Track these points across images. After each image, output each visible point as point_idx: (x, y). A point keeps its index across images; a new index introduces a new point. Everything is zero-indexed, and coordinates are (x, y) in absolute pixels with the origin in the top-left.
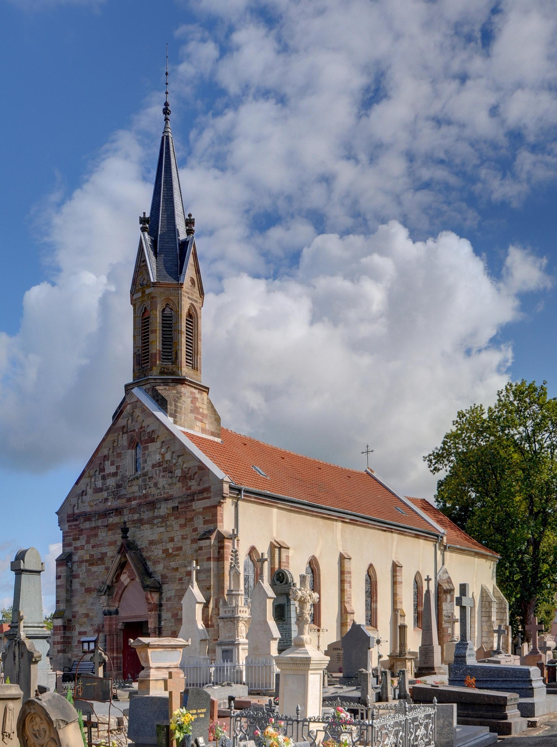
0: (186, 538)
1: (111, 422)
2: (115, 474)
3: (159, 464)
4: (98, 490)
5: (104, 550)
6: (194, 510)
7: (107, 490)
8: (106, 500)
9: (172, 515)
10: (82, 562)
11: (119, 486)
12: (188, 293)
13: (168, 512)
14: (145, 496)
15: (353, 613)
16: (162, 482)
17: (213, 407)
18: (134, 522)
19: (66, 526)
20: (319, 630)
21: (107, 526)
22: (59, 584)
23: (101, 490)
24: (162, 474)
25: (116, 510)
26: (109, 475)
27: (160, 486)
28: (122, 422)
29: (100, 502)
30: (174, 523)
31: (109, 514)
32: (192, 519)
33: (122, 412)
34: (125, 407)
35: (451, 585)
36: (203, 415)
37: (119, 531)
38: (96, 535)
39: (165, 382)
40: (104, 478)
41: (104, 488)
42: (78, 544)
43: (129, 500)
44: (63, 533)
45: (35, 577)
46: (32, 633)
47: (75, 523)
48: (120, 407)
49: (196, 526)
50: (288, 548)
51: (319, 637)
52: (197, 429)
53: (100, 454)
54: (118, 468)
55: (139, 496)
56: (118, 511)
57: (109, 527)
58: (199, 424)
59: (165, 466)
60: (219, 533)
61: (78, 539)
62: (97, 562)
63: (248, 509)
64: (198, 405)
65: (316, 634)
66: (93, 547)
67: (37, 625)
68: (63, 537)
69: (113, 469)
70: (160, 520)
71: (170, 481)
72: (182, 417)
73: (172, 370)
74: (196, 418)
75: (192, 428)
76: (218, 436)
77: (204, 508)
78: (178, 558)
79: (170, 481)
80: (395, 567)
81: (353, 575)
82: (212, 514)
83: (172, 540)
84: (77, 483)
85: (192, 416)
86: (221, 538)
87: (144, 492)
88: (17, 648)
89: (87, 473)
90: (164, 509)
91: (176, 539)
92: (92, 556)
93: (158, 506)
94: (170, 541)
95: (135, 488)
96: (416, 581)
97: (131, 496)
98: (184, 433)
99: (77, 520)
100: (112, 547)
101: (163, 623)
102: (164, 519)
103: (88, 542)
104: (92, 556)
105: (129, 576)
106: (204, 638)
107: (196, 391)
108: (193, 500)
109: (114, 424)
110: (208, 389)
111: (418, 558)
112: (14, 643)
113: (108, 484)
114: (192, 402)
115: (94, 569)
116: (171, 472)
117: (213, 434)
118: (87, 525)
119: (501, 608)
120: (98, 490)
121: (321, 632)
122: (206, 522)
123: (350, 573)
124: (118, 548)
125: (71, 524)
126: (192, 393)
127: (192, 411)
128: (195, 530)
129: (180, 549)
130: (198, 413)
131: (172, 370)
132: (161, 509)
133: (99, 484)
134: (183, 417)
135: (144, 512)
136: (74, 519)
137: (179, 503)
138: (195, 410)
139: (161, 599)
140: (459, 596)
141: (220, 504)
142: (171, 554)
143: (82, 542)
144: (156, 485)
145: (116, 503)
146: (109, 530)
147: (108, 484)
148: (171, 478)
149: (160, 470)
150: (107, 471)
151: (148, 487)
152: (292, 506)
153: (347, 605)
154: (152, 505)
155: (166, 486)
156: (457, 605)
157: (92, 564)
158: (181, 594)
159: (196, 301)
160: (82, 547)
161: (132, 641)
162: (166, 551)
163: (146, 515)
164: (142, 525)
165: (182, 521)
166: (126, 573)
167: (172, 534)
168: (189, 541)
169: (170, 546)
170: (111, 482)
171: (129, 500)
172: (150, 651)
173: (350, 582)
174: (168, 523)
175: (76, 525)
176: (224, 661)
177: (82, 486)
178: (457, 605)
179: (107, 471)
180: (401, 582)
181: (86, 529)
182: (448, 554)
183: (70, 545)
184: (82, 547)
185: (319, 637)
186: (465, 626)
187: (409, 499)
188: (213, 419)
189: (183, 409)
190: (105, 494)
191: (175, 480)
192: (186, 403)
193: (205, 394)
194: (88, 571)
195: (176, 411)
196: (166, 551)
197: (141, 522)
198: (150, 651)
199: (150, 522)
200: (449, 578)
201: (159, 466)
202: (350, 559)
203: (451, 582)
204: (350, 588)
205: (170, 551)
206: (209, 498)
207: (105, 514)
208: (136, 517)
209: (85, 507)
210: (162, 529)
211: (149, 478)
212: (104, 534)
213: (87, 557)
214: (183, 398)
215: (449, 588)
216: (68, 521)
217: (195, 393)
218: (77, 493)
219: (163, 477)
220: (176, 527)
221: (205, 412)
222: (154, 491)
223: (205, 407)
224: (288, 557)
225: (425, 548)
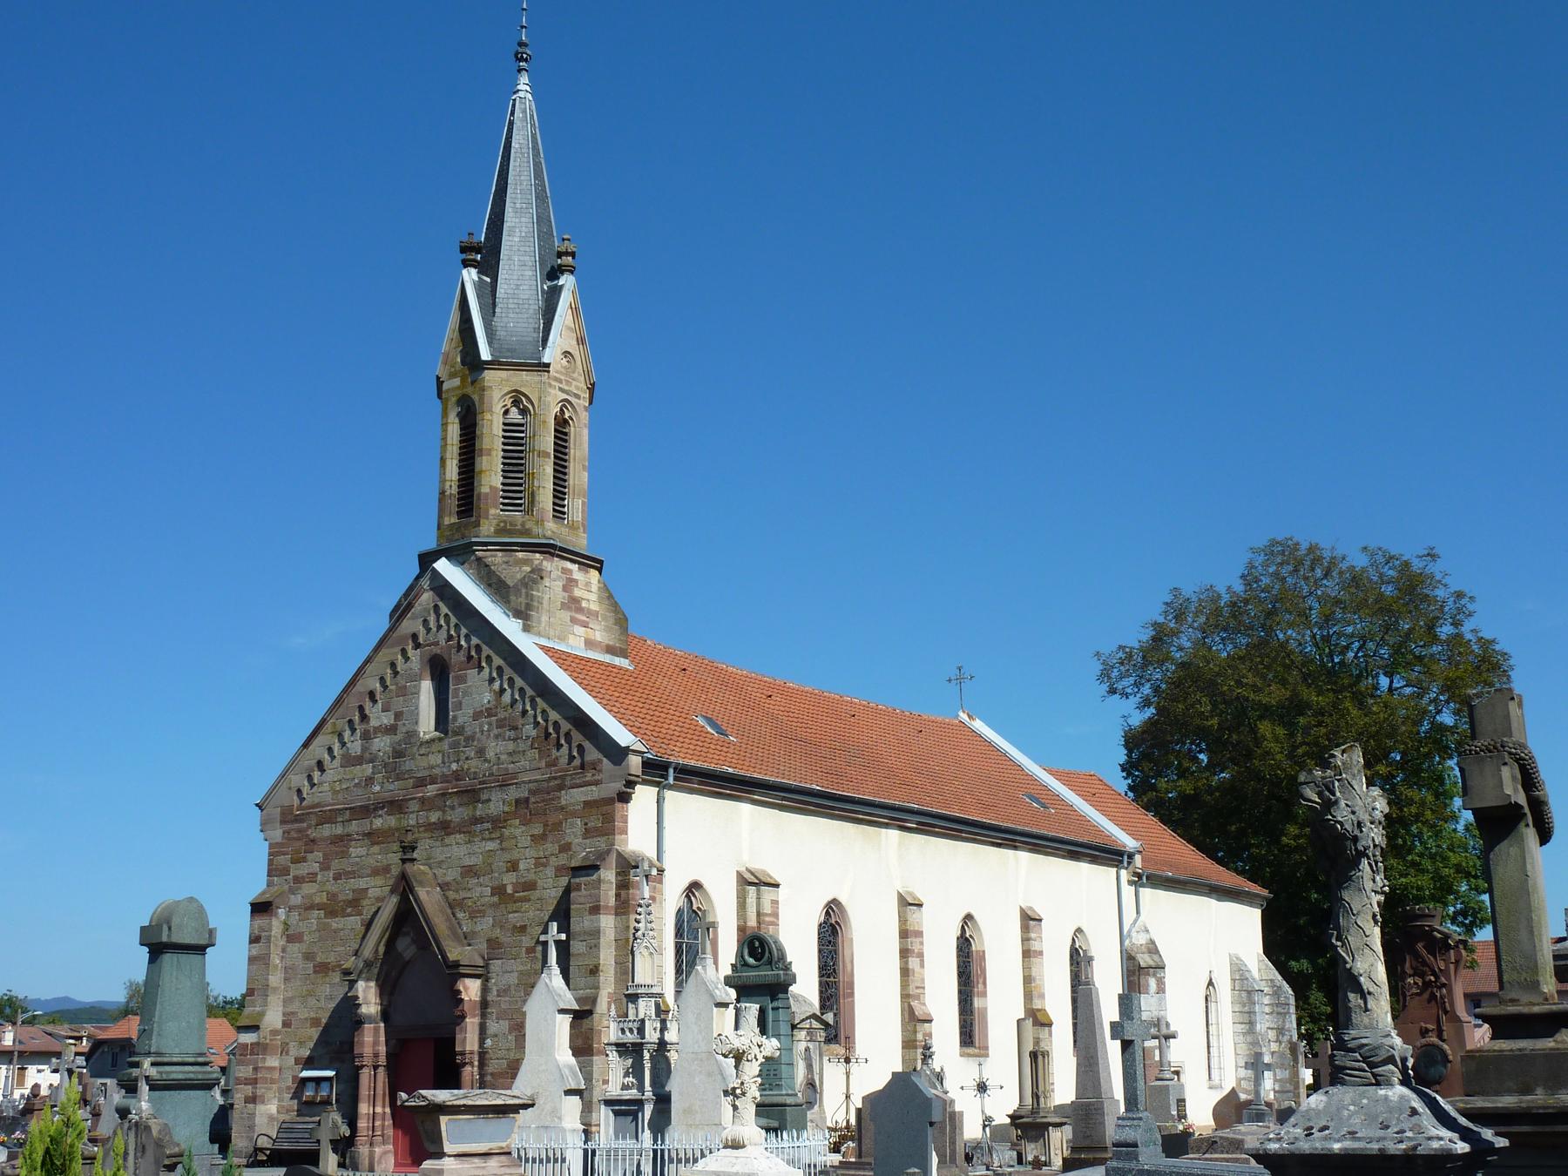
0: (545, 865)
1: (385, 624)
2: (391, 730)
3: (490, 713)
4: (350, 761)
5: (362, 883)
6: (562, 808)
7: (371, 761)
8: (370, 781)
9: (514, 815)
10: (311, 907)
11: (398, 754)
12: (556, 379)
13: (506, 809)
14: (457, 776)
15: (930, 1021)
16: (494, 748)
17: (610, 597)
18: (430, 827)
19: (277, 834)
20: (847, 1061)
21: (369, 835)
22: (254, 952)
23: (359, 760)
24: (496, 731)
25: (391, 803)
26: (377, 730)
27: (490, 754)
28: (410, 625)
29: (356, 785)
30: (518, 832)
31: (375, 809)
32: (558, 826)
33: (410, 606)
34: (417, 596)
35: (1156, 957)
36: (589, 613)
37: (396, 846)
38: (344, 854)
39: (507, 547)
40: (366, 736)
41: (367, 755)
42: (302, 870)
43: (421, 783)
44: (271, 846)
45: (194, 959)
46: (180, 1076)
47: (296, 825)
48: (406, 595)
49: (568, 839)
50: (777, 886)
51: (848, 1074)
52: (572, 640)
53: (361, 687)
54: (398, 716)
55: (444, 775)
56: (396, 806)
57: (372, 837)
58: (579, 630)
59: (501, 715)
60: (619, 854)
61: (304, 860)
62: (343, 910)
63: (686, 807)
64: (577, 593)
65: (842, 1067)
66: (337, 877)
67: (191, 1060)
68: (270, 854)
69: (387, 719)
70: (489, 825)
71: (511, 746)
72: (542, 619)
73: (523, 524)
74: (574, 621)
75: (562, 638)
76: (622, 653)
77: (587, 804)
78: (526, 906)
79: (511, 746)
80: (1029, 920)
81: (927, 938)
82: (605, 815)
83: (513, 866)
84: (306, 745)
85: (565, 616)
86: (628, 866)
87: (454, 766)
88: (132, 1135)
89: (328, 727)
90: (497, 803)
91: (522, 866)
92: (332, 897)
93: (484, 797)
94: (508, 871)
95: (436, 759)
96: (1074, 952)
97: (426, 773)
98: (543, 648)
99: (302, 821)
100: (379, 881)
101: (489, 1042)
102: (498, 823)
103: (325, 867)
104: (332, 897)
105: (414, 941)
106: (573, 1086)
107: (575, 567)
108: (561, 788)
109: (391, 629)
110: (601, 562)
111: (1079, 898)
112: (126, 1125)
113: (374, 748)
114: (565, 589)
115: (335, 923)
116: (515, 728)
117: (610, 650)
118: (327, 831)
119: (1277, 1005)
120: (350, 761)
121: (853, 1066)
122: (588, 833)
123: (919, 934)
124: (391, 882)
125: (288, 827)
126: (565, 571)
127: (564, 606)
128: (565, 848)
129: (530, 886)
130: (580, 610)
131: (523, 524)
132: (492, 805)
133: (355, 747)
134: (544, 618)
135: (453, 808)
136: (296, 826)
137: (530, 791)
138: (573, 604)
139: (485, 990)
140: (1117, 1019)
141: (625, 798)
142: (512, 895)
143: (312, 865)
144: (481, 752)
145: (391, 787)
146: (373, 844)
147: (374, 748)
148: (515, 740)
149: (490, 724)
150: (374, 723)
151: (463, 757)
152: (784, 799)
153: (914, 1004)
154: (471, 795)
155: (503, 757)
156: (1113, 1038)
157: (332, 913)
158: (528, 985)
159: (577, 396)
160: (312, 878)
161: (404, 1095)
162: (499, 891)
163: (458, 814)
164: (448, 834)
165: (537, 829)
166: (407, 934)
167: (515, 855)
168: (550, 872)
169: (509, 880)
170: (382, 744)
171: (421, 783)
172: (444, 1119)
173: (921, 955)
174: (506, 832)
175: (299, 831)
176: (617, 1138)
177: (318, 750)
178: (1113, 1038)
179: (374, 723)
180: (1041, 953)
181: (324, 839)
182: (1146, 893)
183: (284, 872)
184: (312, 878)
185: (848, 1074)
186: (1135, 1081)
187: (1065, 777)
188: (612, 621)
189: (545, 602)
190: (368, 769)
191: (522, 746)
192: (551, 590)
193: (594, 574)
194: (322, 928)
195: (529, 607)
196: (499, 891)
197: (445, 828)
198: (444, 1119)
199: (468, 828)
200: (1153, 942)
201: (490, 715)
202: (920, 905)
203: (1157, 952)
204: (922, 966)
205: (509, 890)
206: (596, 783)
207: (365, 811)
208: (434, 817)
209: (325, 792)
210: (491, 846)
211: (467, 739)
212: (362, 851)
213: (322, 898)
214: (547, 582)
215: (1152, 963)
216: (283, 822)
217: (570, 571)
218: (309, 760)
219: (497, 737)
220: (525, 841)
221: (594, 607)
222: (474, 765)
223: (593, 597)
224: (775, 903)
225: (1098, 879)
